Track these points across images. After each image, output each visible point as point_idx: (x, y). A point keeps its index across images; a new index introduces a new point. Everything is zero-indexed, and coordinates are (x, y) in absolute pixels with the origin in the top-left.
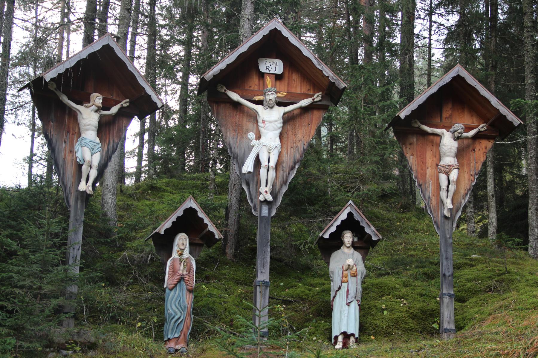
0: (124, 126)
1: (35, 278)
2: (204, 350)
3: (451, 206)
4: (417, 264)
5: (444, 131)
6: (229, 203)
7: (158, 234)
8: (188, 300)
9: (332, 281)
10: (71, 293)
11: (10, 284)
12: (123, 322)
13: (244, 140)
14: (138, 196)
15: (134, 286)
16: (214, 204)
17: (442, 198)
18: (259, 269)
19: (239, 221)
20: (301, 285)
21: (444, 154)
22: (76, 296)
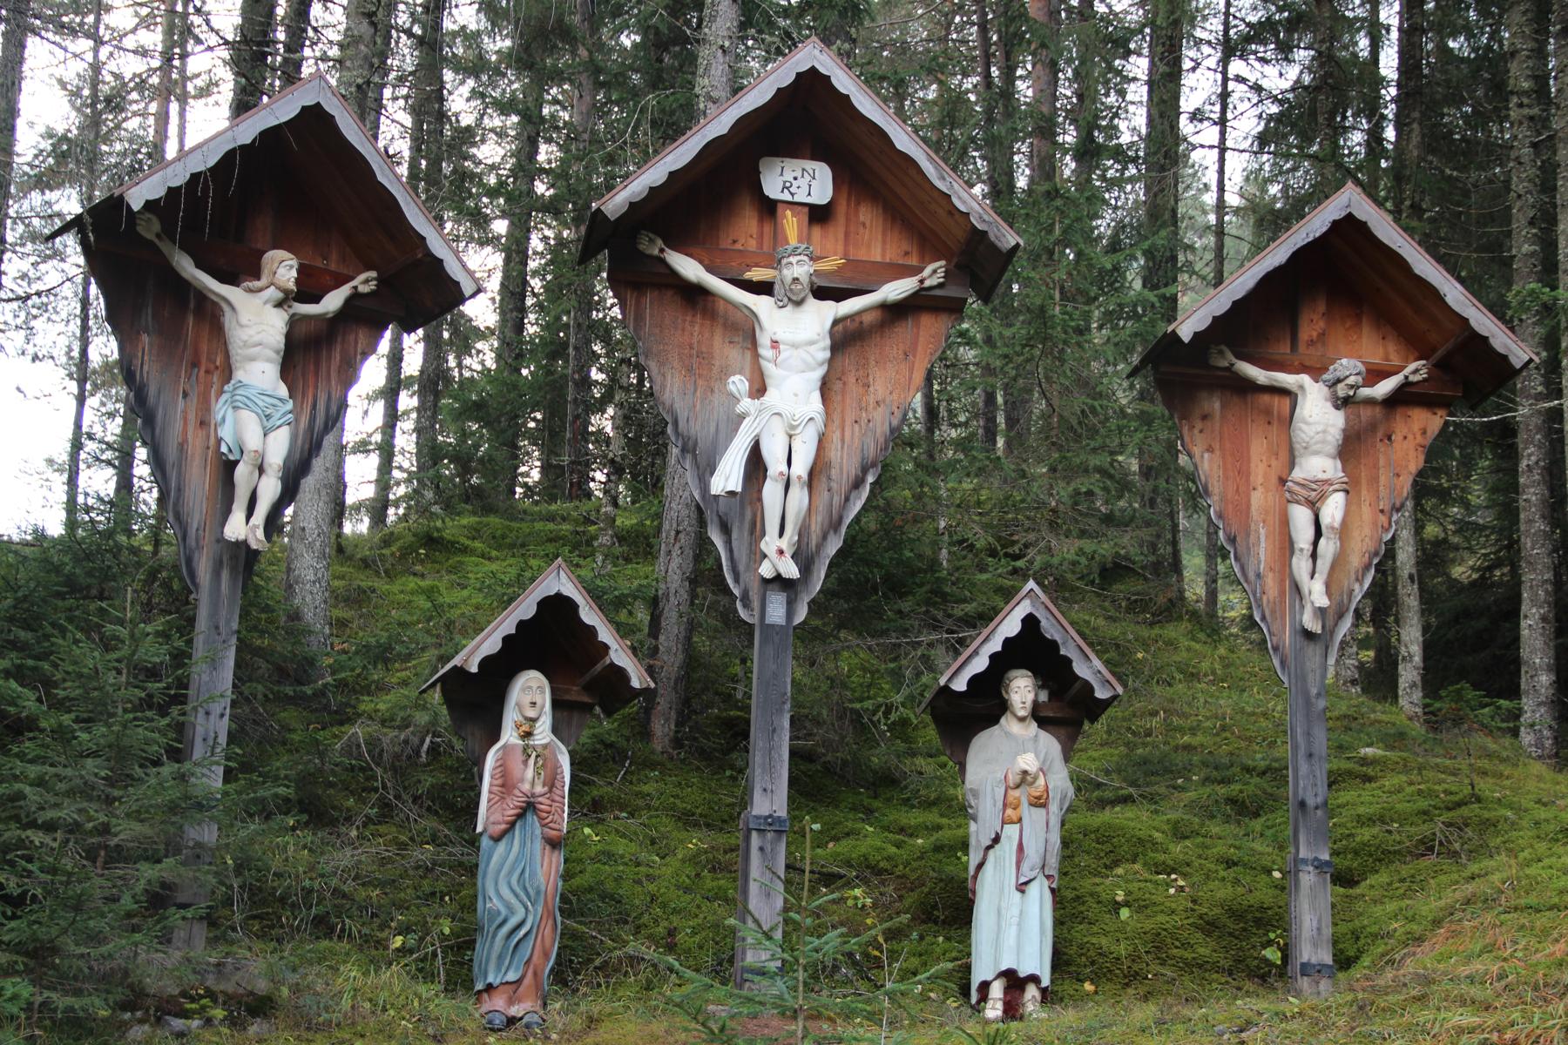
0: (359, 350)
1: (90, 799)
2: (592, 1022)
3: (1322, 601)
4: (1205, 772)
5: (1305, 379)
6: (662, 586)
7: (459, 671)
8: (547, 869)
9: (975, 820)
10: (199, 845)
11: (17, 818)
12: (350, 935)
13: (717, 399)
14: (388, 566)
15: (382, 829)
16: (616, 589)
17: (1298, 578)
18: (757, 779)
19: (688, 639)
20: (871, 829)
21: (1306, 448)
22: (213, 856)
